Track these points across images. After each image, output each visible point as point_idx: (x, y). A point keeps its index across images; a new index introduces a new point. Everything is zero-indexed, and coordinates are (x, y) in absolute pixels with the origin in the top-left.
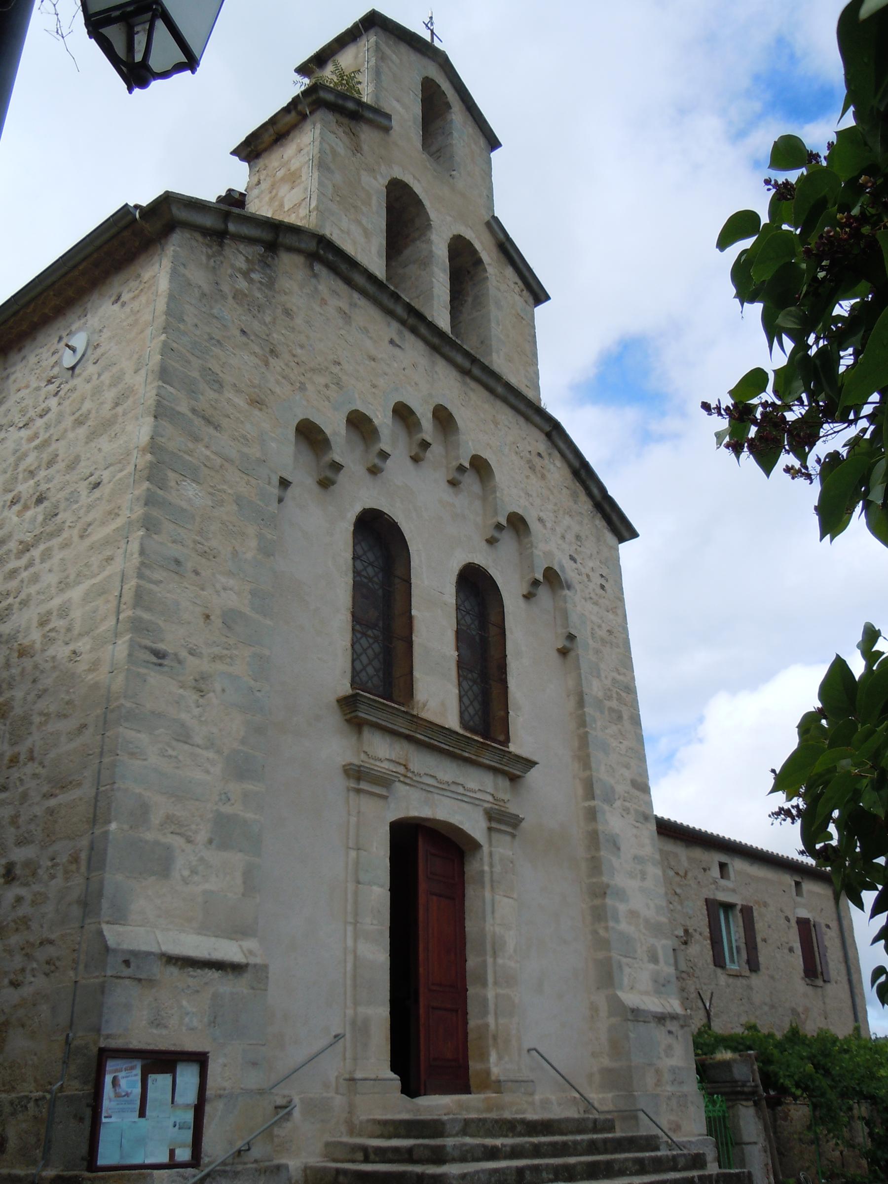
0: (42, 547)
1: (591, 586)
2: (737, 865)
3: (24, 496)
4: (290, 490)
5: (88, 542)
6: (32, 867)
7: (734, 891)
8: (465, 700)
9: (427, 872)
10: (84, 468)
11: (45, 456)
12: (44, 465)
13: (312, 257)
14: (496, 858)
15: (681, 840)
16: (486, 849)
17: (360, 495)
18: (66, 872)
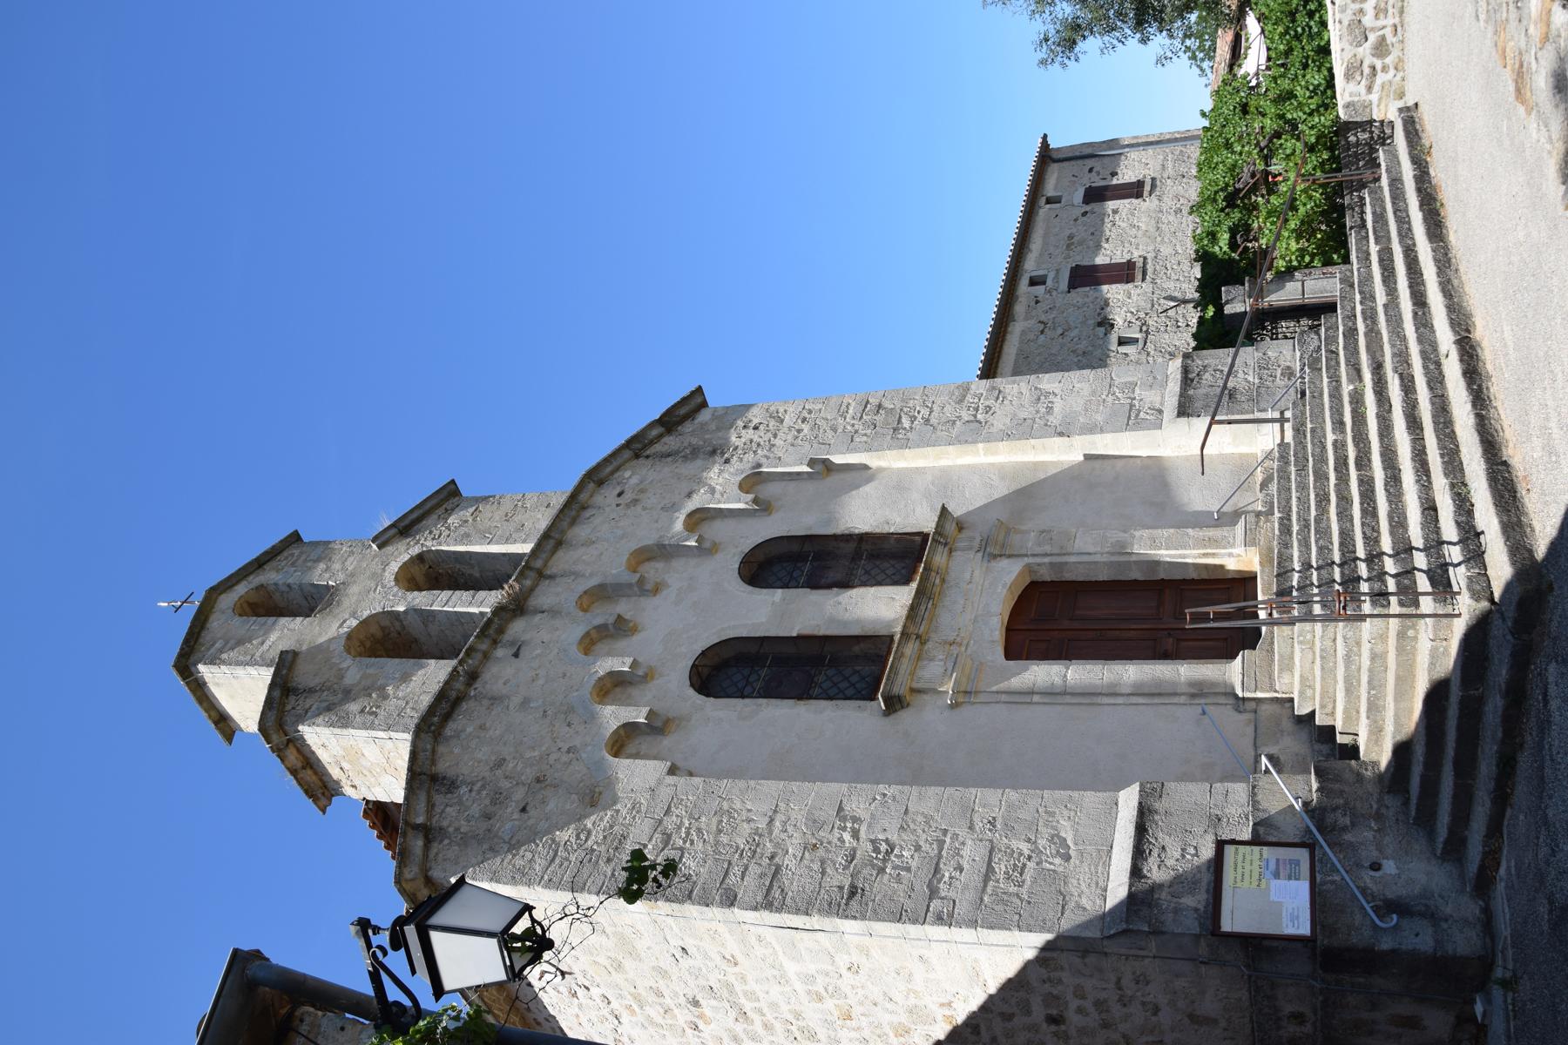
0: (743, 1001)
1: (756, 439)
2: (1030, 266)
3: (690, 1018)
4: (679, 764)
5: (740, 958)
6: (1050, 999)
7: (1058, 271)
8: (879, 578)
10: (666, 963)
11: (652, 998)
12: (661, 1000)
13: (437, 736)
14: (1038, 550)
15: (1007, 326)
18: (1056, 969)
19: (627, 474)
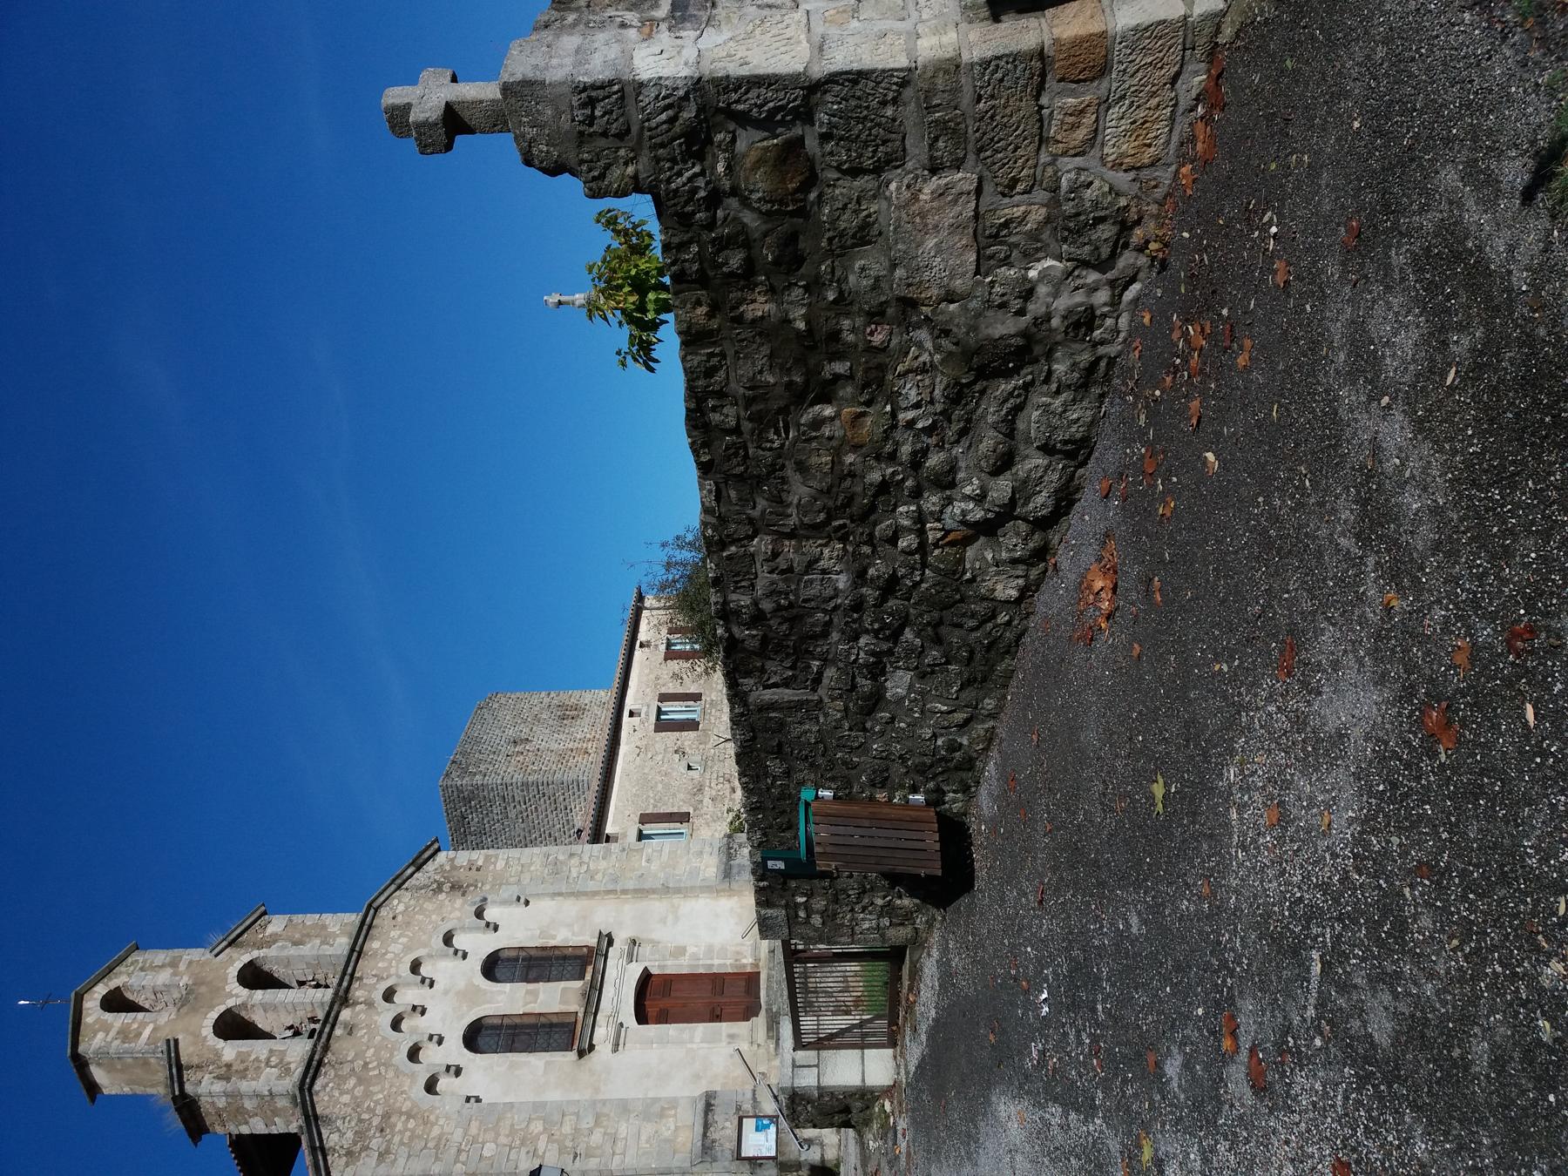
2: (630, 703)
9: (658, 999)
16: (646, 964)
19: (395, 902)
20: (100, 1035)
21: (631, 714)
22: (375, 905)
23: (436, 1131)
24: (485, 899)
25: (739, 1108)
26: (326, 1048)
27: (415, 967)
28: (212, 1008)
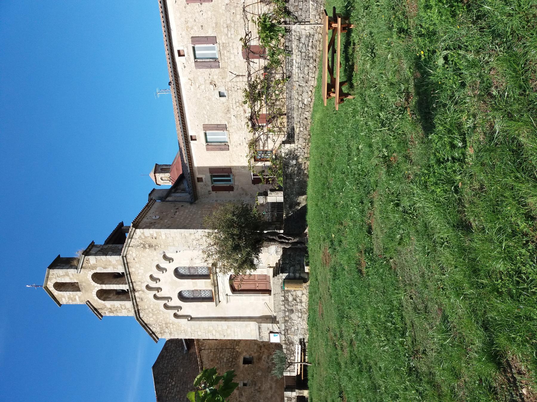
17: (176, 302)
20: (63, 299)
21: (180, 55)
22: (124, 255)
23: (182, 329)
24: (164, 252)
25: (268, 329)
26: (137, 305)
27: (151, 277)
28: (92, 291)
